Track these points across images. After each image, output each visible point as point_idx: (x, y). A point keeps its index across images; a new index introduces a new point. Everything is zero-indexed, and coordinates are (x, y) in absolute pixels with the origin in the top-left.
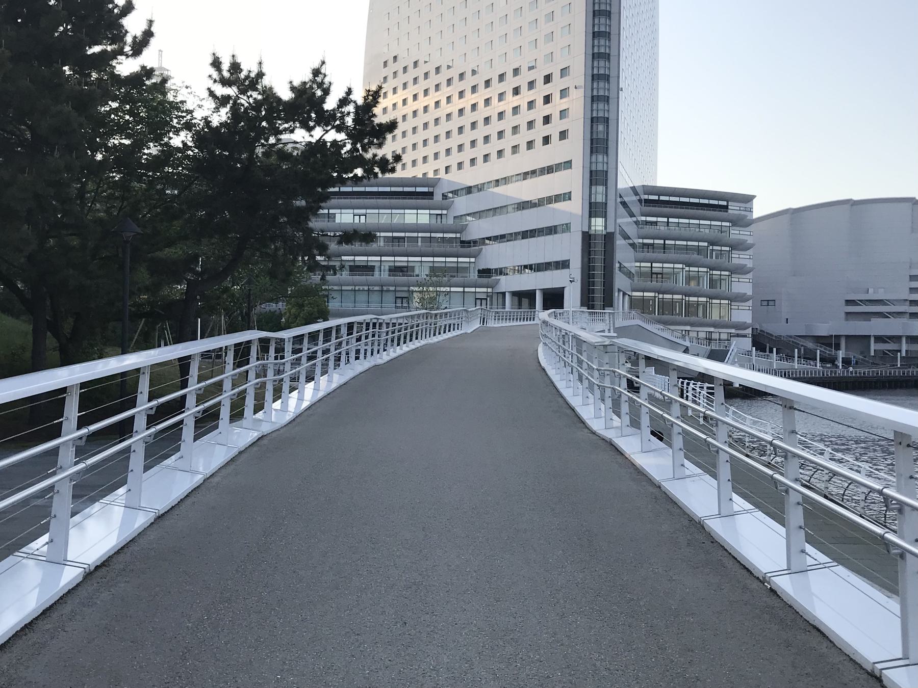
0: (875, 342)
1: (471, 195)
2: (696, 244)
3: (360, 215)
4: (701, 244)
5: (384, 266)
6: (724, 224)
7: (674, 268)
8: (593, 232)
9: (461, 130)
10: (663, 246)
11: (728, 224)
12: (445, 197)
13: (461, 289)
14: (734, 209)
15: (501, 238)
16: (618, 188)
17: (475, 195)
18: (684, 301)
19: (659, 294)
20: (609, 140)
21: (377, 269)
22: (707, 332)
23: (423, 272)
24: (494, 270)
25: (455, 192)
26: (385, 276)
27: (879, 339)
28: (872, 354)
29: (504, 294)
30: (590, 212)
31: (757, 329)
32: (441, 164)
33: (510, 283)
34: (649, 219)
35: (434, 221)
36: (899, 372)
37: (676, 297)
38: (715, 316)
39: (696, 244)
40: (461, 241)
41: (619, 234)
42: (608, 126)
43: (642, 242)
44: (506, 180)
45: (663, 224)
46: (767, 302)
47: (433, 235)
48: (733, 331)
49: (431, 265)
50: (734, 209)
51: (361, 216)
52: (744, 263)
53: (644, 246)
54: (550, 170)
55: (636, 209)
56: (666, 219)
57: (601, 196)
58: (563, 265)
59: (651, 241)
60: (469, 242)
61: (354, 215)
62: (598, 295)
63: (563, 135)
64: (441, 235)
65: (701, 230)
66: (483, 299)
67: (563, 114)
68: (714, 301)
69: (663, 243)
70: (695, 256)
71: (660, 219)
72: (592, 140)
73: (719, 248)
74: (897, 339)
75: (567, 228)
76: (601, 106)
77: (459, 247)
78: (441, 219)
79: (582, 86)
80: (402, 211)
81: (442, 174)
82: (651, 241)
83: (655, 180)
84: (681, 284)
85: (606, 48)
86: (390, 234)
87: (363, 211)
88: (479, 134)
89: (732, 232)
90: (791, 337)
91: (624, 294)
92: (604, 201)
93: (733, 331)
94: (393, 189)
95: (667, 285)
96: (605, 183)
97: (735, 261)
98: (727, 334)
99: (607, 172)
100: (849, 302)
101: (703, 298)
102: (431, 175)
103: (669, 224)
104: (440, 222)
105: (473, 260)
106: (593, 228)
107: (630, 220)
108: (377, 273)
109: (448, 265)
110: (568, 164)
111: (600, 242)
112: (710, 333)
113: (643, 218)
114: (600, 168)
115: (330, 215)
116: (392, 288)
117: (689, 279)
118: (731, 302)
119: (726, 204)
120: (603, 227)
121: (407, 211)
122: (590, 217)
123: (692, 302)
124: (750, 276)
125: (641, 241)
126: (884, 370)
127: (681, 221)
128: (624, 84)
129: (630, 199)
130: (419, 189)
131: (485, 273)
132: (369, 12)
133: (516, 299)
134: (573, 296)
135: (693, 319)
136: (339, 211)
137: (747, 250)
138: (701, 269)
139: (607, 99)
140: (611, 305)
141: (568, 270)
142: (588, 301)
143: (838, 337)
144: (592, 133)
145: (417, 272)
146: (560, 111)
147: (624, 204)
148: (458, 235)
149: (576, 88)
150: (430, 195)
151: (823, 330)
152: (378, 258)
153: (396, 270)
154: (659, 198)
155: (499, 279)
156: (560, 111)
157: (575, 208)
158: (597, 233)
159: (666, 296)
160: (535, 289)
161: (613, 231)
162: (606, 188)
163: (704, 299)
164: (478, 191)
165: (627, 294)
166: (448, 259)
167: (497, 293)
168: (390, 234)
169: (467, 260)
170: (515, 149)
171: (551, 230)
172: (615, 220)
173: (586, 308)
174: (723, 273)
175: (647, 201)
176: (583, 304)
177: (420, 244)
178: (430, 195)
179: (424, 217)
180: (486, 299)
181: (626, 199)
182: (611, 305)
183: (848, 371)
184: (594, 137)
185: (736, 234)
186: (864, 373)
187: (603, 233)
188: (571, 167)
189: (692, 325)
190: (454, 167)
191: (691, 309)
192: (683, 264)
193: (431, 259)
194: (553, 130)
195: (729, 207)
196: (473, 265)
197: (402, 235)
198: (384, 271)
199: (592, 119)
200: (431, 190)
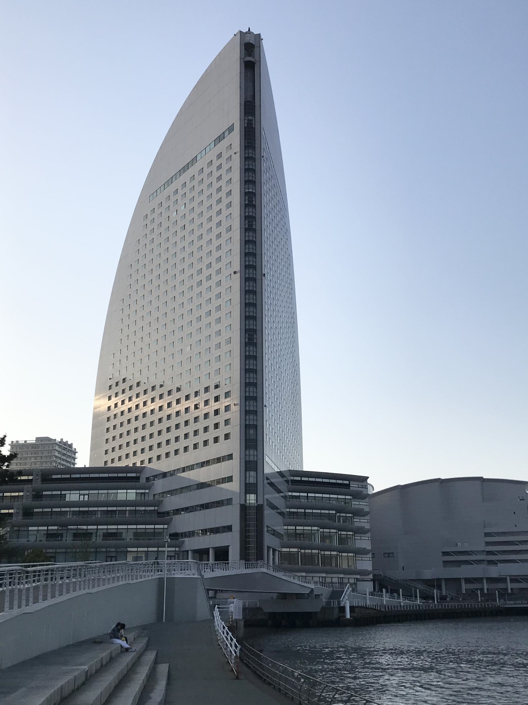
0: (465, 583)
1: (166, 478)
2: (327, 512)
3: (84, 495)
4: (331, 512)
5: (100, 533)
6: (347, 497)
7: (304, 530)
8: (248, 505)
9: (160, 433)
10: (304, 513)
11: (349, 497)
12: (148, 479)
13: (156, 549)
14: (354, 486)
15: (186, 509)
16: (265, 473)
17: (168, 479)
18: (320, 554)
19: (301, 549)
20: (258, 440)
21: (94, 535)
22: (355, 578)
23: (129, 537)
24: (180, 534)
25: (155, 476)
26: (99, 540)
27: (468, 581)
28: (464, 592)
29: (187, 551)
30: (246, 490)
31: (381, 575)
32: (145, 457)
33: (190, 544)
34: (294, 494)
35: (139, 498)
36: (481, 605)
37: (314, 551)
38: (345, 566)
39: (327, 512)
40: (158, 512)
41: (267, 505)
42: (256, 430)
43: (289, 511)
44: (191, 468)
45: (312, 498)
46: (388, 554)
47: (138, 508)
48: (358, 577)
49: (135, 531)
50: (354, 486)
51: (85, 496)
52: (363, 526)
53: (291, 514)
54: (219, 460)
55: (283, 487)
56: (306, 494)
57: (252, 478)
58: (229, 528)
59: (295, 510)
60: (164, 513)
61: (80, 495)
62: (253, 551)
63: (227, 436)
64: (143, 508)
65: (331, 502)
66: (173, 556)
67: (227, 422)
68: (343, 554)
69: (304, 511)
70: (326, 521)
71: (302, 494)
72: (246, 440)
73: (344, 515)
74: (479, 580)
75: (229, 502)
76: (252, 417)
77: (156, 517)
78: (145, 496)
79: (238, 404)
80: (115, 491)
81: (146, 464)
82: (295, 510)
83: (302, 466)
84: (318, 541)
85: (254, 380)
86: (105, 509)
87: (87, 492)
88: (190, 429)
89: (353, 503)
90: (406, 580)
91: (274, 550)
92: (255, 482)
93: (358, 577)
94: (111, 475)
95: (307, 542)
96: (256, 470)
97: (356, 524)
98: (353, 579)
99: (257, 462)
100: (445, 554)
101: (345, 554)
102: (138, 465)
103: (309, 497)
104: (143, 499)
105: (166, 526)
106: (248, 502)
107: (277, 495)
108: (64, 539)
109: (147, 531)
110: (230, 457)
111: (253, 511)
112: (339, 578)
113: (290, 494)
114: (252, 458)
115: (62, 495)
116: (104, 550)
117: (323, 538)
118: (355, 555)
119: (348, 483)
120: (255, 501)
121: (119, 491)
122: (246, 494)
123: (307, 554)
124: (369, 535)
125: (288, 510)
126: (469, 604)
127: (317, 495)
128: (268, 402)
129: (277, 480)
130: (129, 475)
131: (175, 536)
132: (101, 352)
133: (197, 555)
134: (234, 553)
135: (328, 568)
136: (69, 492)
137: (366, 516)
138: (332, 531)
139: (255, 413)
140: (262, 558)
141: (231, 532)
142: (245, 556)
143: (439, 580)
144: (246, 435)
145: (124, 536)
146: (225, 420)
147: (271, 484)
148: (156, 508)
149: (235, 405)
150: (137, 479)
151: (428, 575)
152: (95, 527)
153: (108, 535)
154: (301, 479)
155: (184, 541)
156: (225, 420)
157: (235, 487)
158: (251, 505)
159: (307, 551)
160: (208, 547)
161: (262, 503)
162: (257, 473)
163: (335, 553)
164: (171, 476)
165: (277, 550)
166: (148, 527)
167: (183, 551)
168: (105, 509)
169: (162, 526)
170: (206, 443)
171: (219, 504)
172: (263, 496)
173: (244, 561)
174: (348, 533)
175: (293, 482)
176: (241, 558)
177: (127, 515)
178: (137, 479)
179: (131, 495)
180: (175, 556)
181: (273, 481)
182: (262, 558)
183: (442, 605)
184: (248, 438)
185: (356, 504)
186: (452, 606)
187: (255, 505)
188: (232, 459)
189: (327, 572)
190: (155, 459)
191: (327, 560)
192: (58, 526)
193: (134, 527)
194: (221, 433)
195: (351, 485)
196: (166, 530)
197: (115, 509)
198: (100, 537)
199: (246, 425)
200: (138, 475)
